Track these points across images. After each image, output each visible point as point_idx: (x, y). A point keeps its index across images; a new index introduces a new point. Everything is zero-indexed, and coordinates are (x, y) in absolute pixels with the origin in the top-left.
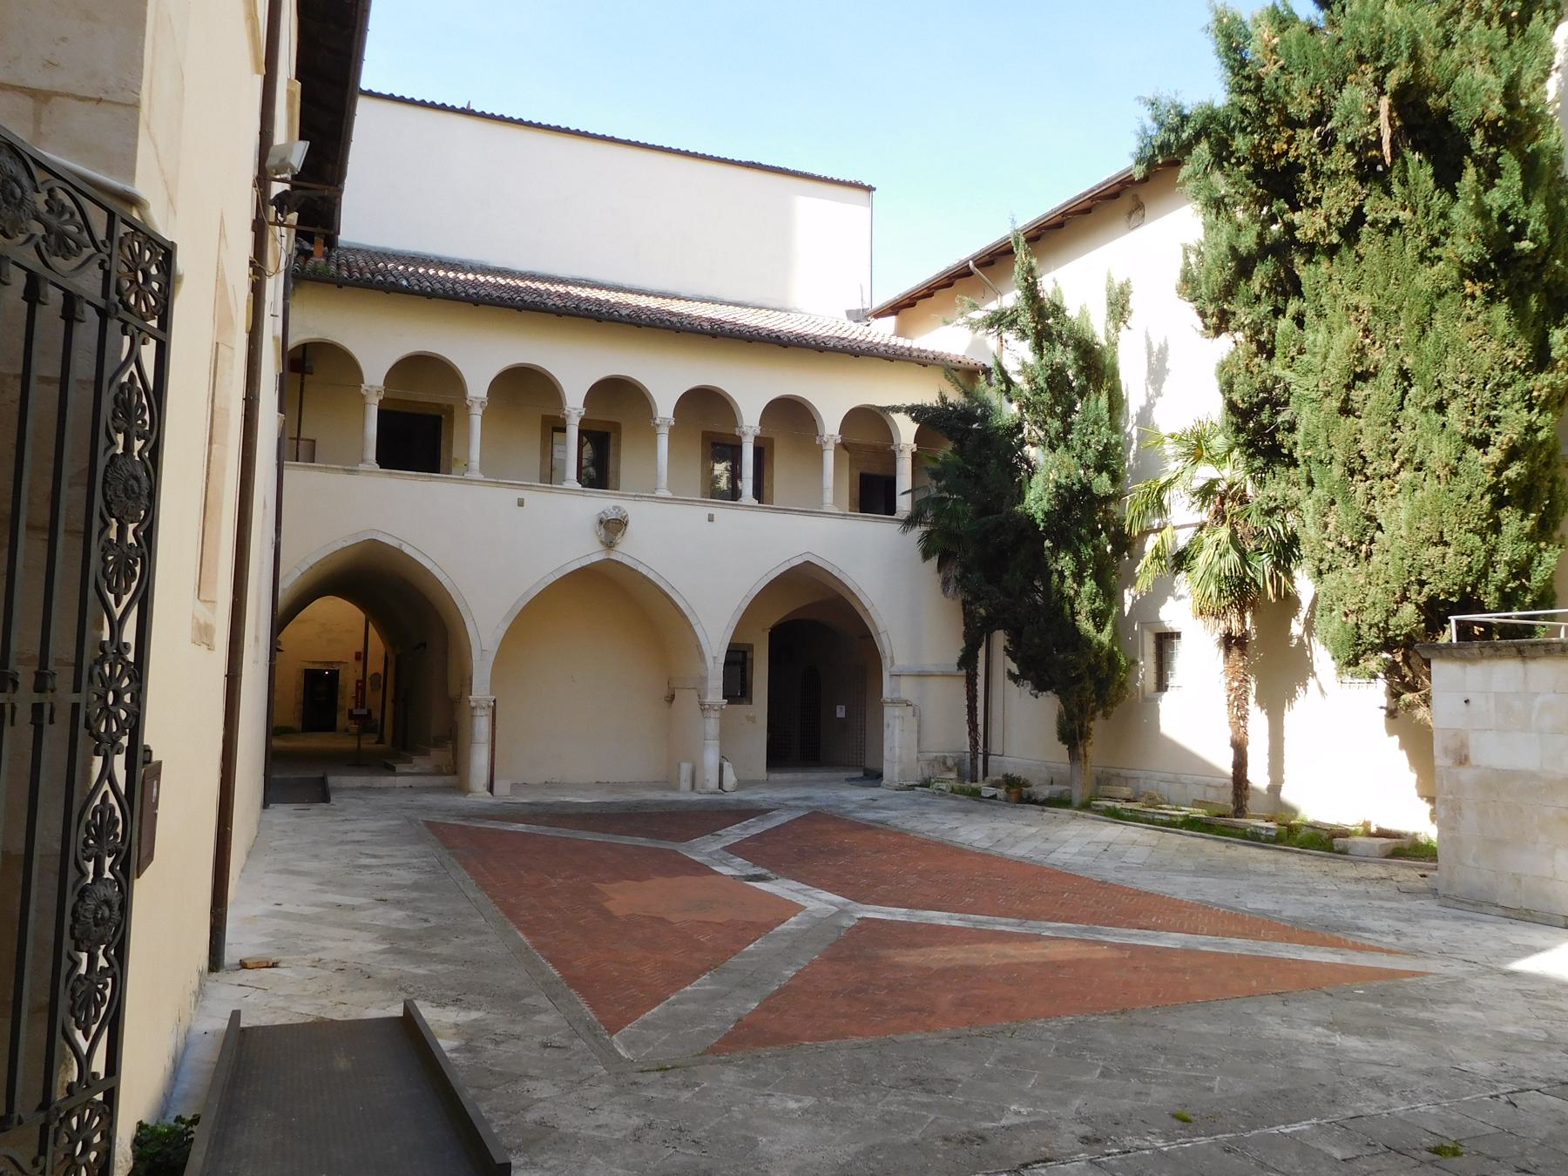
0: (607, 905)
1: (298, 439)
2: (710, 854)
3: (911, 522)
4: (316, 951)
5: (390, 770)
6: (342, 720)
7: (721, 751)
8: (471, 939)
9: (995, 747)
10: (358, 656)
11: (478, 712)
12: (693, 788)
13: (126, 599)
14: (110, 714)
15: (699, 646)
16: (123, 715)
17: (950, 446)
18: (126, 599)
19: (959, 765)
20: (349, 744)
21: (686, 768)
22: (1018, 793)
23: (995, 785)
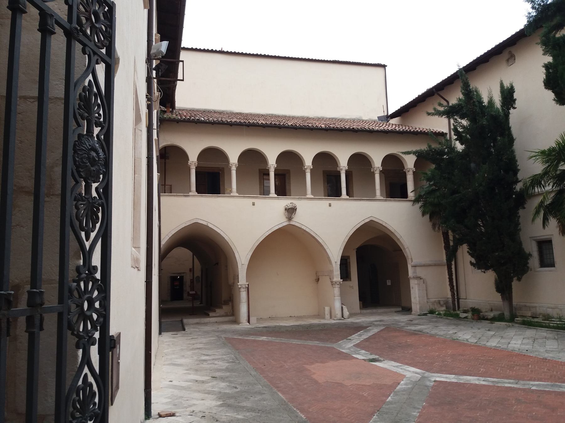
0: (314, 376)
1: (165, 185)
2: (349, 349)
3: (416, 201)
4: (190, 406)
5: (207, 315)
6: (185, 296)
7: (338, 301)
8: (259, 397)
9: (462, 295)
10: (190, 270)
11: (242, 290)
12: (331, 318)
13: (93, 235)
14: (85, 317)
15: (329, 258)
16: (95, 316)
17: (433, 166)
18: (93, 235)
19: (446, 303)
20: (189, 305)
21: (327, 309)
22: (477, 315)
23: (465, 312)
